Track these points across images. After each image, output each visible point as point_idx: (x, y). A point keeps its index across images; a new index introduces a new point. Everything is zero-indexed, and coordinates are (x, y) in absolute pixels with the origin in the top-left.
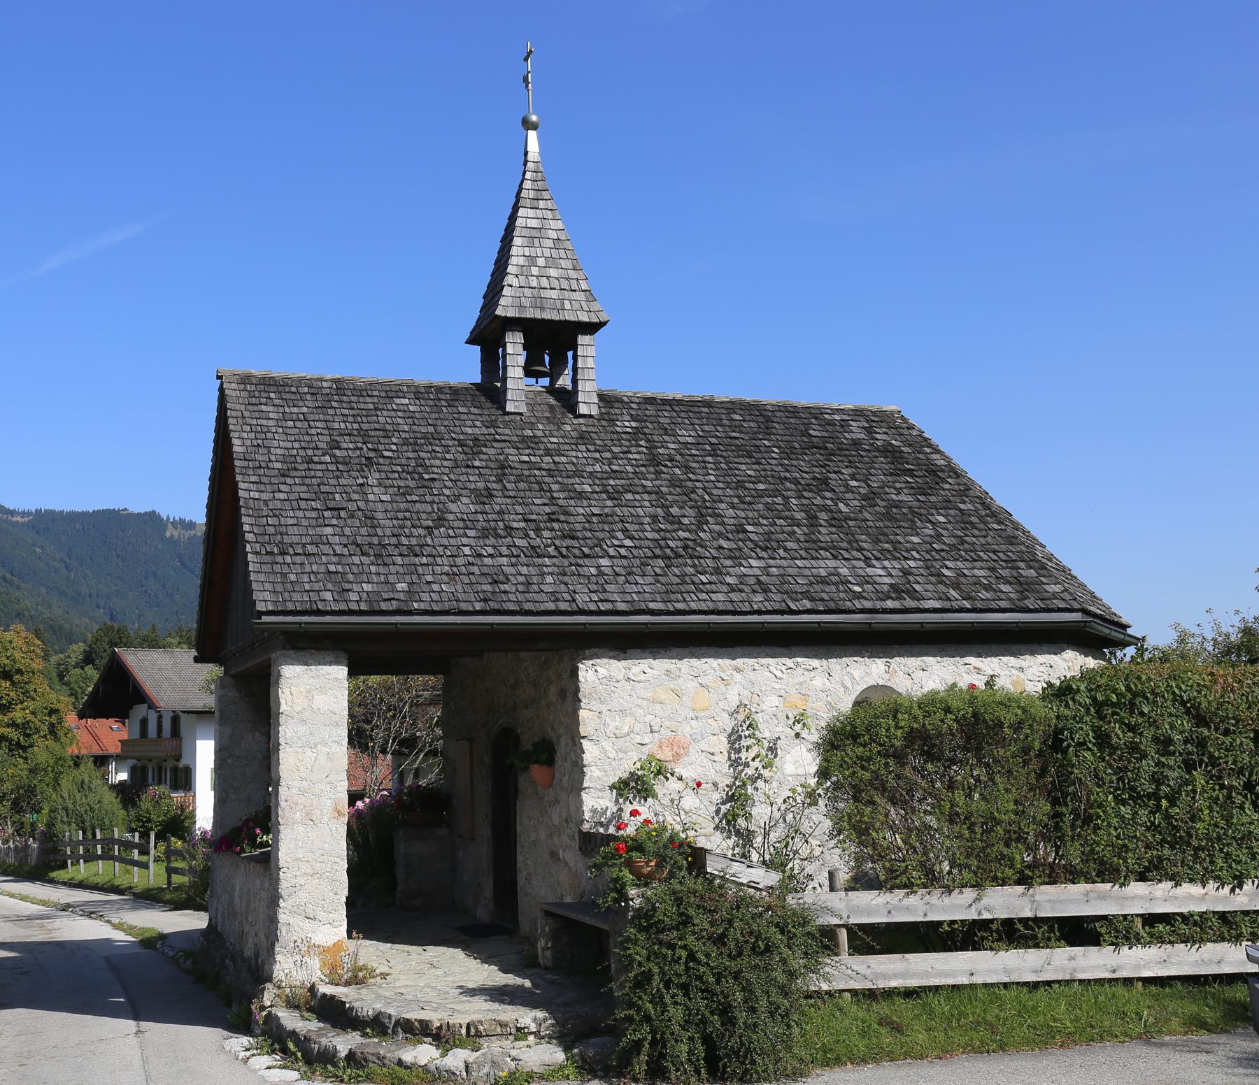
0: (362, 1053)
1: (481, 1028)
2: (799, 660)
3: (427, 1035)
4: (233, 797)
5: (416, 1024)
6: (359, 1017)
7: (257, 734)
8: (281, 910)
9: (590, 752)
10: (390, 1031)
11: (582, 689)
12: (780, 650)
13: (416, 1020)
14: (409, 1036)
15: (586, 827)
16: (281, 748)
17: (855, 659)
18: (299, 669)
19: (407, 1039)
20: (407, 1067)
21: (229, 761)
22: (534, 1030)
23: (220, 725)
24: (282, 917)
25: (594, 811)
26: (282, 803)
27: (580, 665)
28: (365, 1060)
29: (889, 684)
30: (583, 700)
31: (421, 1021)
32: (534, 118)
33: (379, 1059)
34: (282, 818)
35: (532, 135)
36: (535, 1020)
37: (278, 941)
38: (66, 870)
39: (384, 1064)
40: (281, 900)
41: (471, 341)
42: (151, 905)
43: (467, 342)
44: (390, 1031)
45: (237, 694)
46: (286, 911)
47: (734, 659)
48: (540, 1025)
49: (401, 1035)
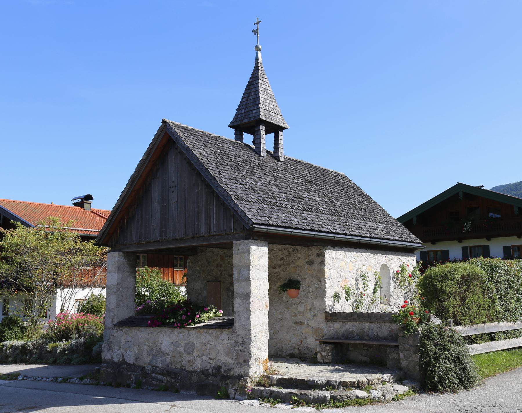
0: (340, 396)
1: (373, 381)
2: (370, 254)
3: (353, 387)
4: (122, 305)
5: (349, 383)
6: (319, 384)
7: (131, 277)
8: (251, 347)
9: (328, 284)
10: (336, 387)
11: (326, 261)
12: (353, 249)
13: (349, 381)
14: (345, 388)
15: (327, 311)
16: (251, 280)
17: (380, 255)
18: (256, 247)
19: (344, 389)
20: (360, 399)
21: (121, 289)
22: (388, 380)
23: (118, 273)
24: (252, 349)
25: (328, 305)
26: (251, 302)
27: (325, 252)
28: (342, 398)
29: (386, 264)
30: (326, 265)
31: (350, 382)
32: (260, 47)
33: (348, 397)
34: (252, 309)
35: (259, 52)
36: (387, 376)
37: (250, 359)
38: (231, 330)
39: (350, 399)
40: (251, 342)
41: (231, 126)
42: (347, 338)
43: (164, 122)
44: (336, 387)
45: (124, 260)
46: (253, 347)
47: (357, 253)
48: (389, 378)
49: (342, 388)
